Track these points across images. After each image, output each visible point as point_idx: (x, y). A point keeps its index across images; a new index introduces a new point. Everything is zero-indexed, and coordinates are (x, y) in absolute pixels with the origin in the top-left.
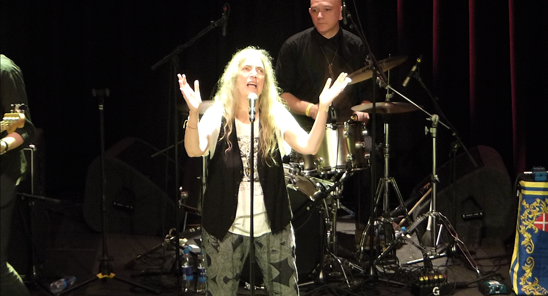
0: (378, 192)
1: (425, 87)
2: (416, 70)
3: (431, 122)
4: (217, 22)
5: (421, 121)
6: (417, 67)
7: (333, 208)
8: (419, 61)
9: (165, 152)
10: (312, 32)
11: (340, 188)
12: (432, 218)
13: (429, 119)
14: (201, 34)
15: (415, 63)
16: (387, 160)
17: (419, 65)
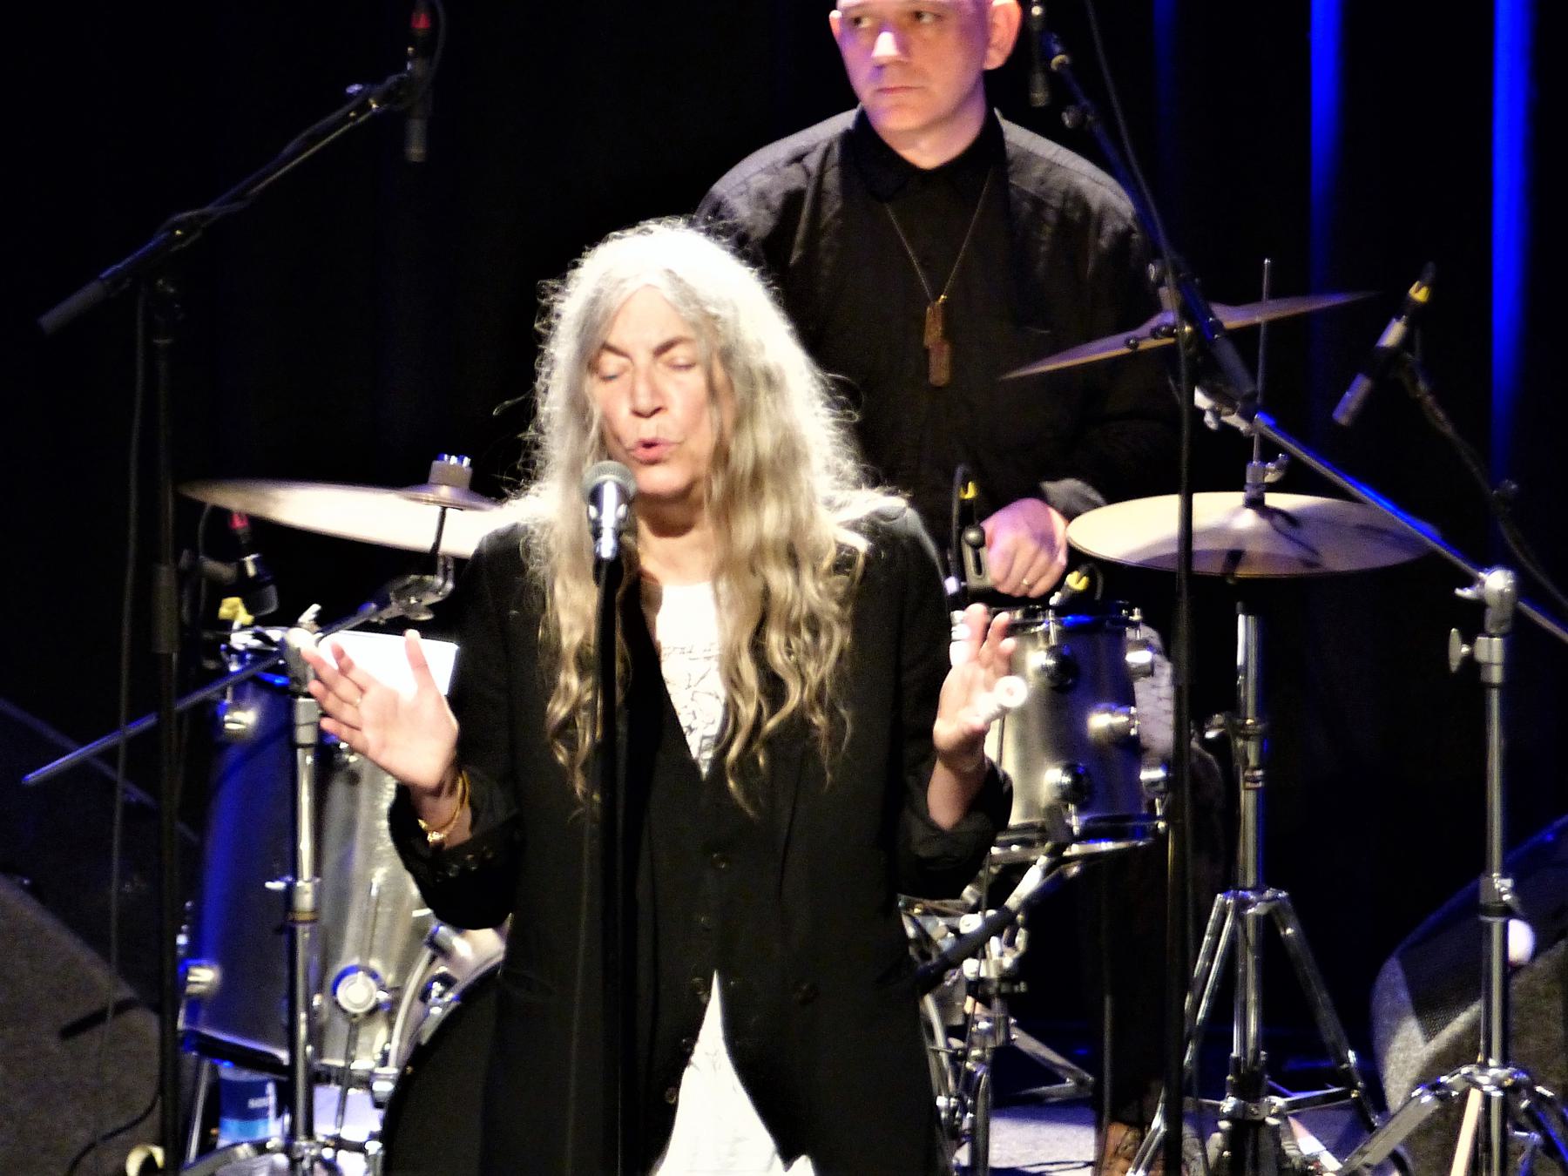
0: (1207, 966)
1: (1448, 429)
2: (1406, 342)
3: (1478, 607)
4: (379, 89)
5: (1421, 601)
6: (1410, 325)
7: (971, 1045)
8: (1419, 294)
9: (109, 755)
10: (847, 138)
11: (1011, 943)
12: (1487, 1099)
13: (1467, 593)
14: (297, 154)
15: (1397, 305)
16: (1248, 800)
17: (1418, 317)
